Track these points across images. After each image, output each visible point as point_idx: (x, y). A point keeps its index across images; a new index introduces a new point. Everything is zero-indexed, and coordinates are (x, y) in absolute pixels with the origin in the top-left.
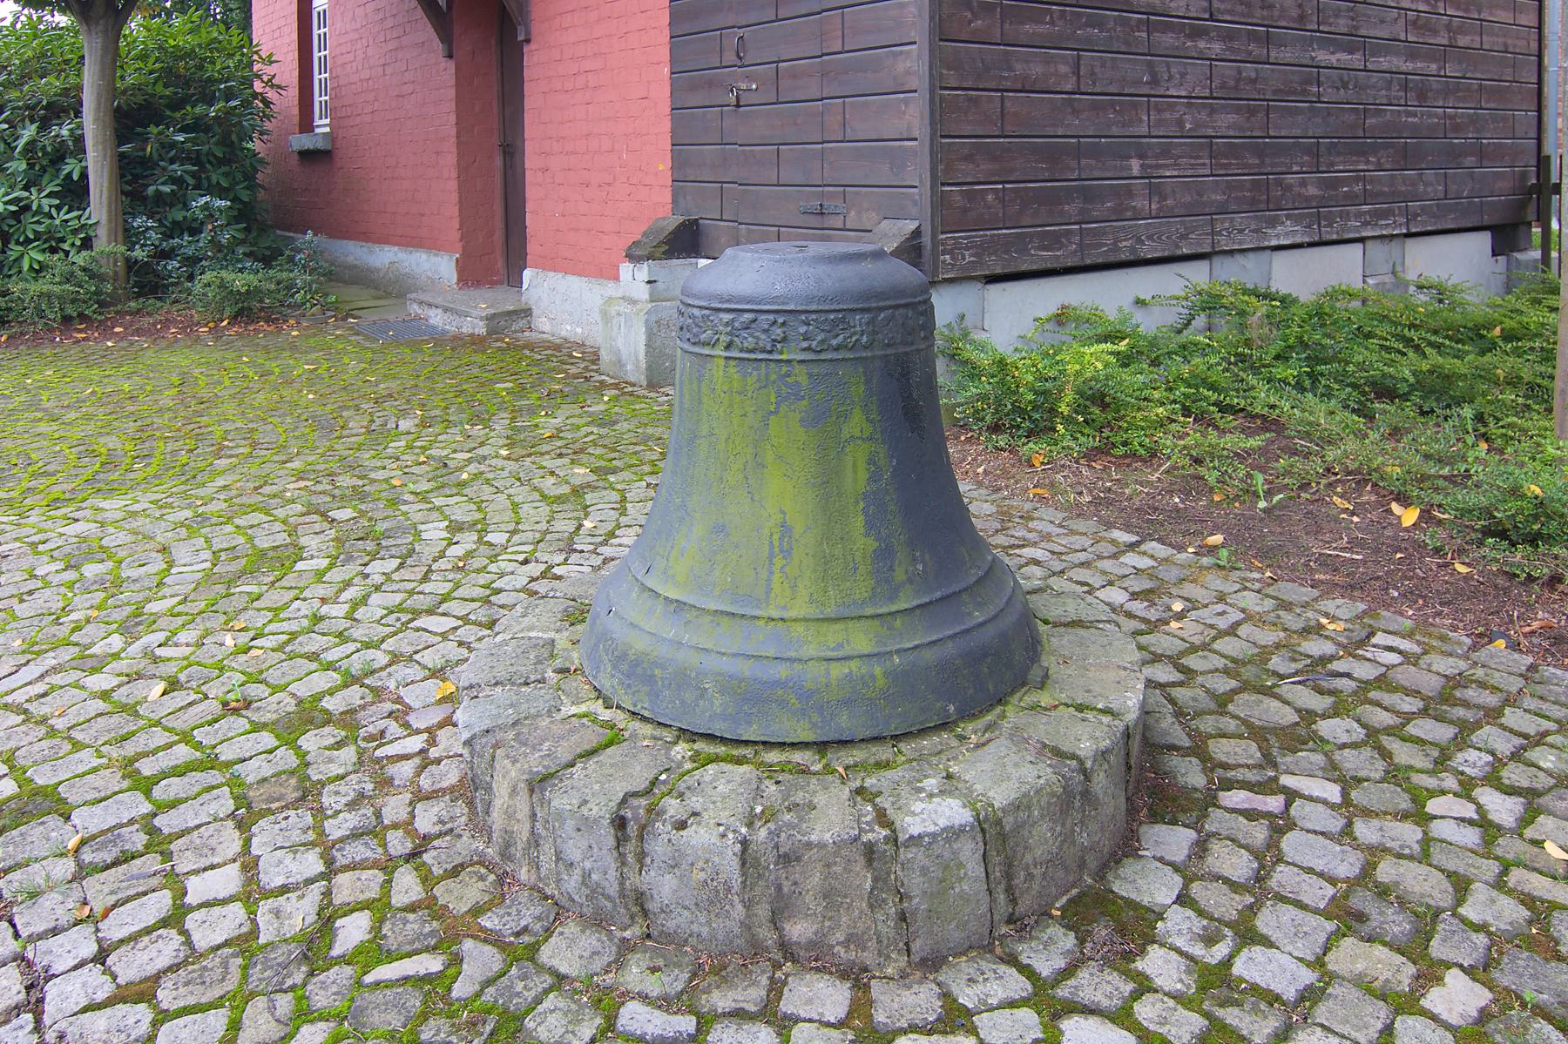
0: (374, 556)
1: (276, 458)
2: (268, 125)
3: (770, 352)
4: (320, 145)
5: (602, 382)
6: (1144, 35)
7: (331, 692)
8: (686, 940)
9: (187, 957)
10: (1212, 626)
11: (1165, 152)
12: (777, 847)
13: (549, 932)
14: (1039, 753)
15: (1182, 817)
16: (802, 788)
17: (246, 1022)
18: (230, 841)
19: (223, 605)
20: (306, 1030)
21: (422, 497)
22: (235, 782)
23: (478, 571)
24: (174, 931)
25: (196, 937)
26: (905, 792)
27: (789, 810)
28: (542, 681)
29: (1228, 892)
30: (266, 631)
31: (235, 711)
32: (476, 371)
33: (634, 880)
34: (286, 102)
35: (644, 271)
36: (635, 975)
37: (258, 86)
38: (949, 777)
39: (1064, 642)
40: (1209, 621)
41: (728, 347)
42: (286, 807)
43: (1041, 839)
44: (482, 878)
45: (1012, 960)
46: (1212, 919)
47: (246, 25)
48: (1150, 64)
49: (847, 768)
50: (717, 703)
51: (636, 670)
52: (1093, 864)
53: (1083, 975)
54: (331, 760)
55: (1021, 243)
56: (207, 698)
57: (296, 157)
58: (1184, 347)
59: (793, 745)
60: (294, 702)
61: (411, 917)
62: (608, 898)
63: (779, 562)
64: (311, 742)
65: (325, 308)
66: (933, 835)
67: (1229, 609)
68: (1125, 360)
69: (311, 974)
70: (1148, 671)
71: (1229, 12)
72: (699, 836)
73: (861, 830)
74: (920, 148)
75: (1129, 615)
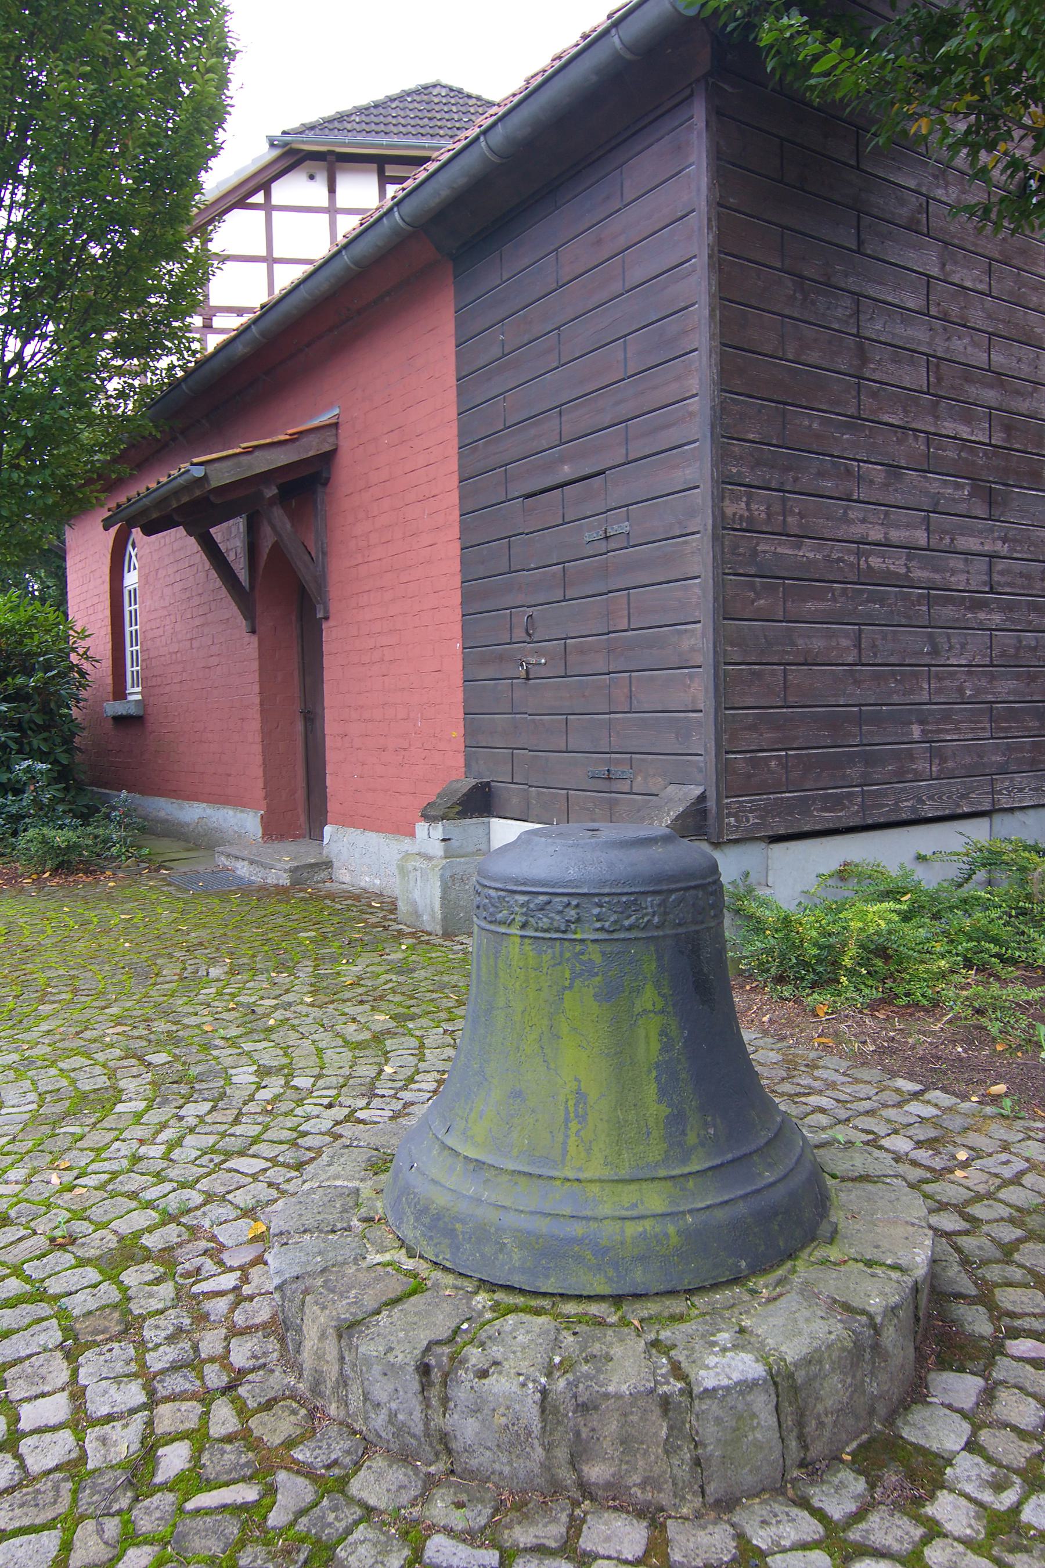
0: (188, 1099)
1: (96, 1004)
2: (83, 693)
3: (564, 932)
4: (133, 711)
5: (399, 931)
6: (925, 608)
7: (150, 1230)
8: (489, 1477)
9: (21, 1480)
10: (996, 1175)
11: (946, 717)
12: (575, 1396)
13: (358, 1466)
14: (830, 1308)
15: (969, 1365)
16: (599, 1339)
17: (77, 1543)
18: (59, 1372)
19: (48, 1145)
20: (132, 1552)
21: (232, 1042)
22: (62, 1314)
23: (286, 1114)
24: (9, 1456)
25: (29, 1461)
26: (698, 1344)
27: (587, 1361)
28: (348, 1229)
29: (1016, 1439)
30: (89, 1170)
31: (62, 1247)
32: (280, 921)
33: (438, 1421)
34: (101, 672)
35: (438, 831)
36: (440, 1508)
37: (74, 658)
38: (742, 1331)
39: (853, 1196)
40: (993, 1170)
41: (524, 926)
42: (110, 1339)
43: (833, 1391)
44: (294, 1412)
45: (804, 1503)
46: (1000, 1466)
47: (61, 603)
48: (931, 636)
49: (641, 1321)
50: (516, 1257)
51: (439, 1224)
52: (882, 1410)
53: (874, 1519)
54: (151, 1295)
55: (803, 805)
56: (35, 1233)
57: (111, 722)
58: (965, 901)
59: (589, 1298)
60: (115, 1239)
61: (228, 1447)
62: (414, 1436)
63: (574, 1126)
64: (131, 1277)
65: (140, 860)
66: (727, 1388)
67: (1013, 1158)
68: (906, 917)
69: (136, 1499)
70: (934, 1220)
71: (1009, 585)
72: (500, 1385)
73: (656, 1382)
74: (705, 718)
75: (915, 1163)
